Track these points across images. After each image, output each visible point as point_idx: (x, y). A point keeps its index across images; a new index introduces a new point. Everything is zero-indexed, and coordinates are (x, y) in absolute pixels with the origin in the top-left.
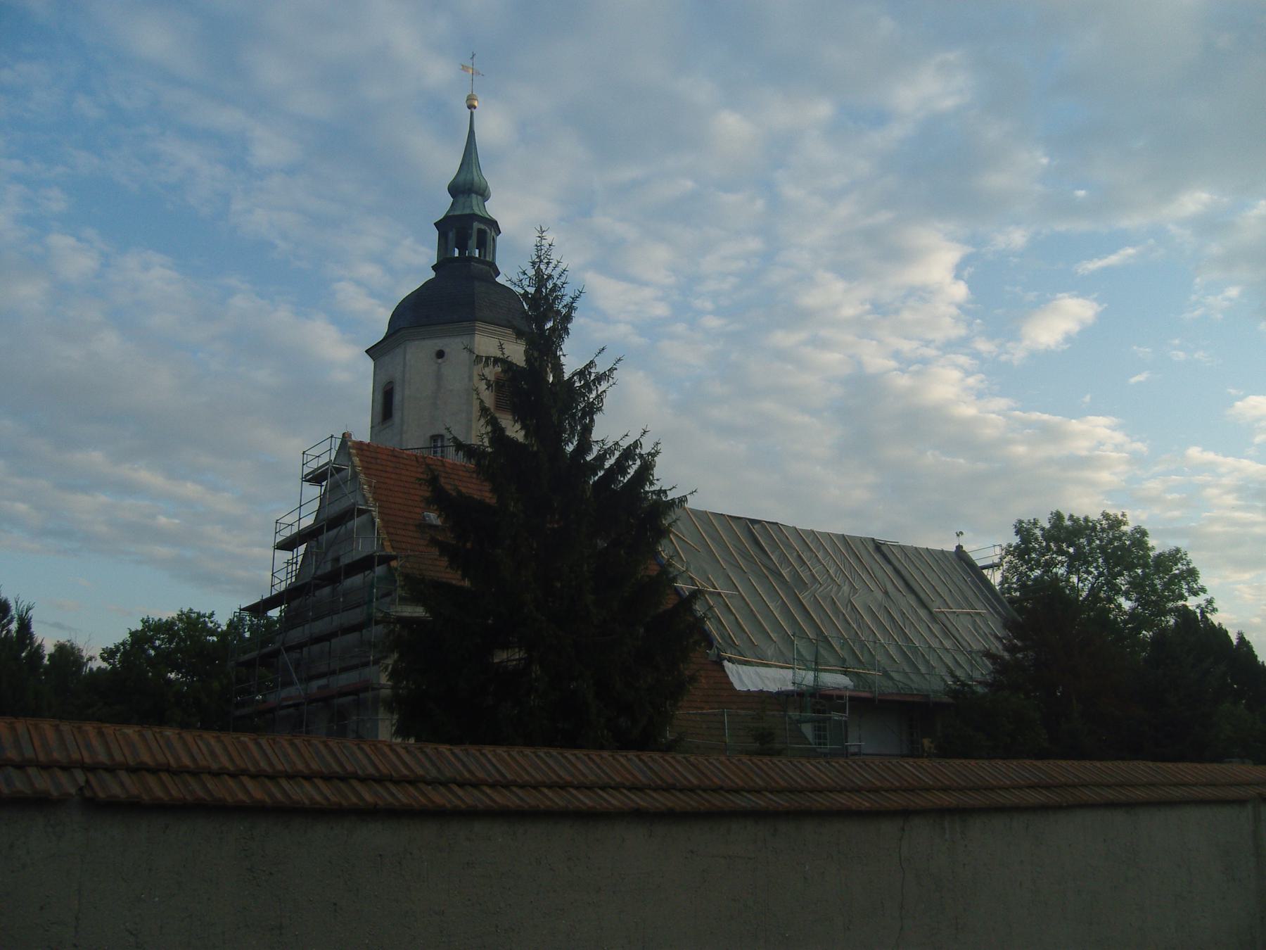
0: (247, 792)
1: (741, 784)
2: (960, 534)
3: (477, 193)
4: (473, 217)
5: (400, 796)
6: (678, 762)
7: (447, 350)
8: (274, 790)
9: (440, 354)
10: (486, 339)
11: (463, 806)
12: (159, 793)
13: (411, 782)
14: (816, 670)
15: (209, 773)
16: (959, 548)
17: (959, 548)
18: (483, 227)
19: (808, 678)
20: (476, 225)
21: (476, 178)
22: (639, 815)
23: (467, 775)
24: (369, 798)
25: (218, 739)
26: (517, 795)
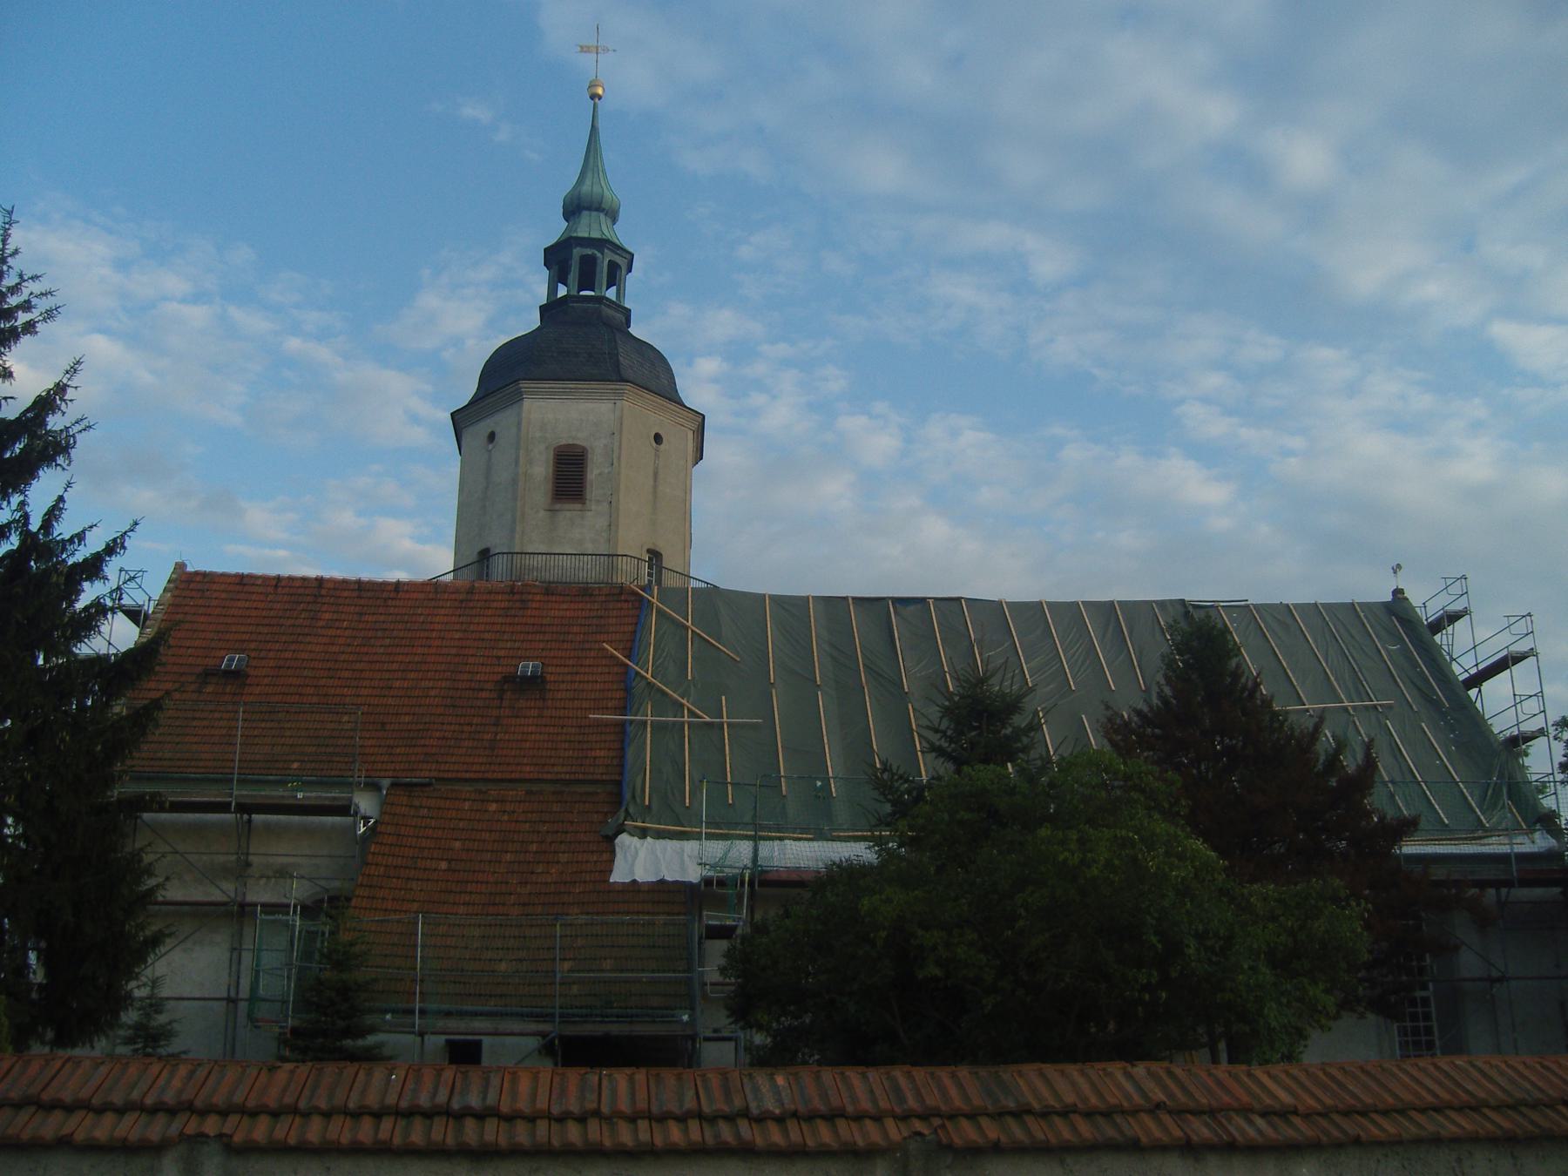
0: (1165, 1129)
1: (1446, 1096)
2: (1397, 568)
3: (589, 209)
4: (603, 243)
5: (1464, 1123)
6: (1423, 1070)
7: (497, 430)
8: (1519, 1119)
9: (492, 437)
10: (542, 403)
11: (1499, 1133)
12: (1157, 1133)
13: (1436, 1110)
14: (755, 839)
15: (988, 1115)
16: (1398, 592)
17: (1398, 592)
18: (589, 251)
19: (741, 851)
20: (577, 252)
21: (607, 193)
22: (1393, 1144)
23: (1390, 1100)
24: (1506, 1124)
25: (1083, 1073)
26: (1376, 1124)
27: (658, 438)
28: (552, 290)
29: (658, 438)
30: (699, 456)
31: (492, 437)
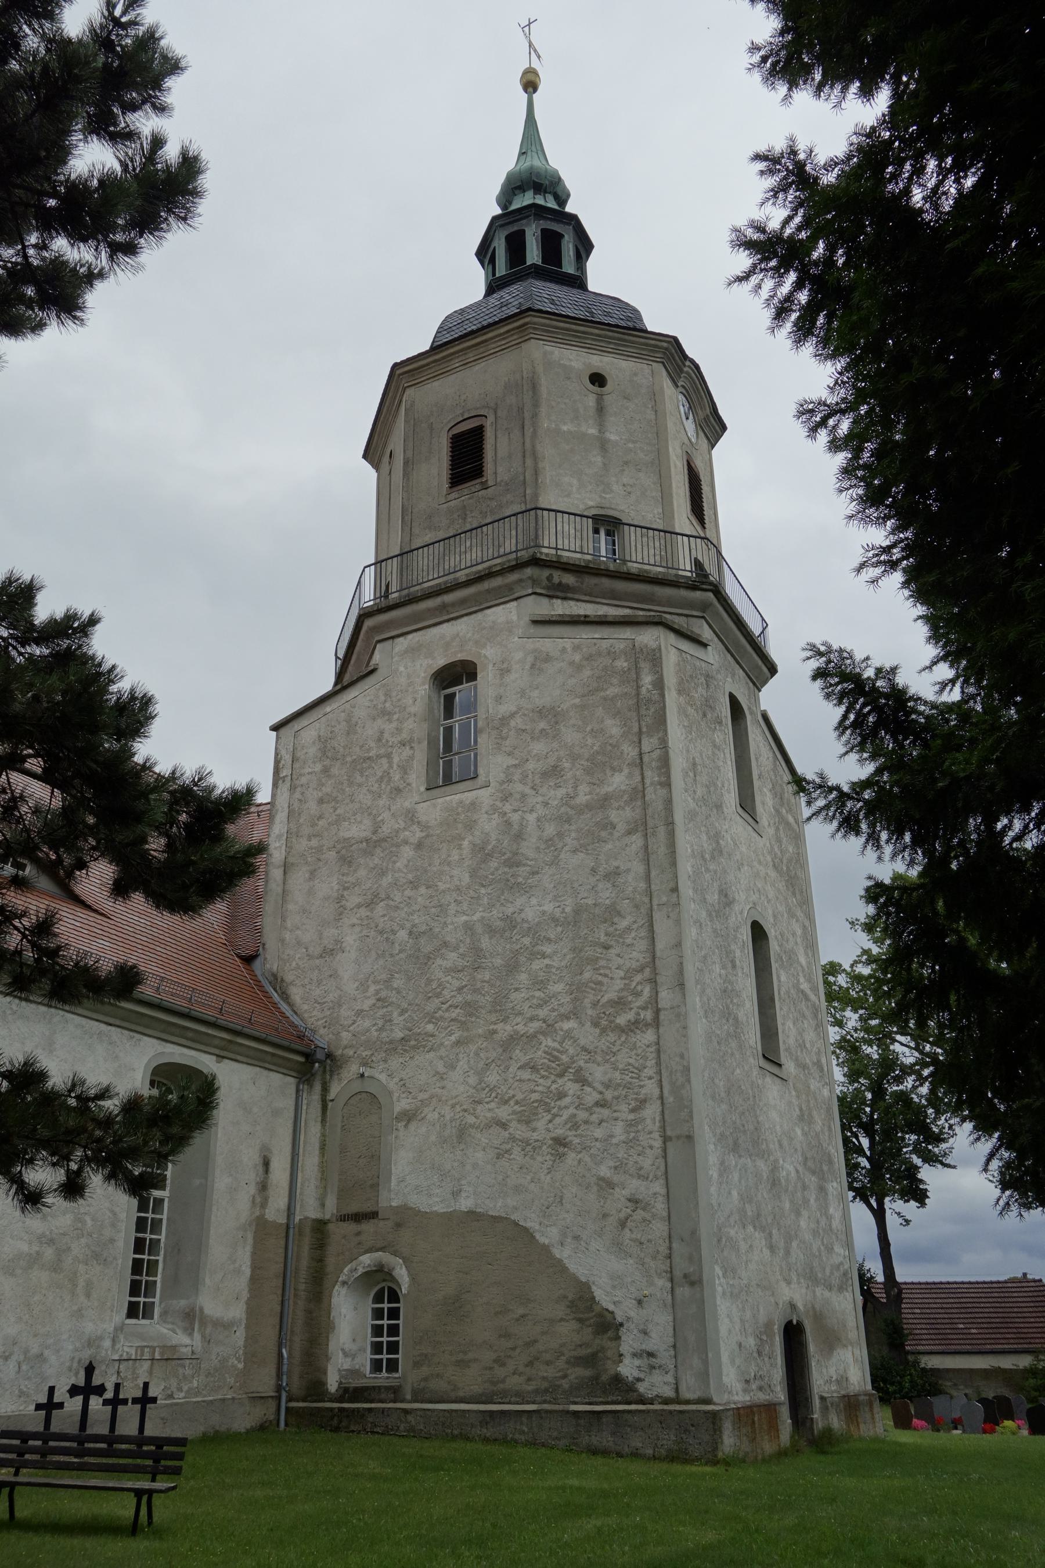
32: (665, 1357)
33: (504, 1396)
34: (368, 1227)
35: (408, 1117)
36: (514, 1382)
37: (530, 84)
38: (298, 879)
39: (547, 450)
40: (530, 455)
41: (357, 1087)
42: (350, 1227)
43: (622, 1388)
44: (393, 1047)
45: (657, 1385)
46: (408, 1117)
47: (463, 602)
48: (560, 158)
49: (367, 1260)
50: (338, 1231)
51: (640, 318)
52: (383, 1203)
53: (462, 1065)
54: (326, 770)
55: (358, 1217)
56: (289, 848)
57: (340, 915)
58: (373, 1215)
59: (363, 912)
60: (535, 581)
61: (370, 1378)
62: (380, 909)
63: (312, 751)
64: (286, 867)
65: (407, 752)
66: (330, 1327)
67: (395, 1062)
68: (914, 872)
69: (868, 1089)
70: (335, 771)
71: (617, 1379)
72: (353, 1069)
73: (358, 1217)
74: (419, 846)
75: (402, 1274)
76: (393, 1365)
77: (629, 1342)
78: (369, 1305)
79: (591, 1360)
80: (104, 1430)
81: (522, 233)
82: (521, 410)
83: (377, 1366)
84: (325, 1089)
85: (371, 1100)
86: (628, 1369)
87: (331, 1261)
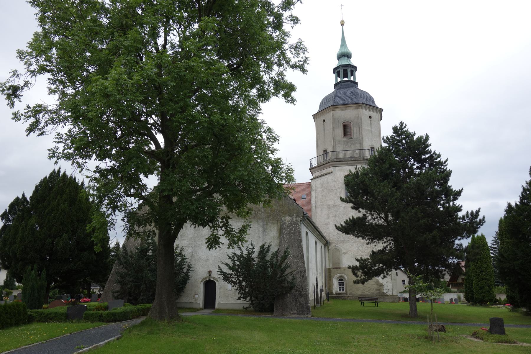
9: (324, 121)
27: (370, 117)
28: (336, 79)
29: (370, 117)
30: (381, 119)
31: (324, 121)
32: (391, 290)
33: (365, 295)
34: (339, 270)
35: (345, 253)
36: (366, 293)
37: (343, 25)
38: (319, 210)
39: (364, 133)
40: (360, 133)
41: (335, 247)
42: (336, 270)
43: (384, 293)
44: (341, 242)
45: (389, 293)
46: (345, 253)
47: (351, 163)
48: (351, 48)
49: (339, 275)
50: (333, 270)
51: (373, 101)
52: (341, 266)
53: (355, 246)
54: (323, 190)
55: (337, 268)
56: (316, 204)
57: (328, 218)
58: (340, 268)
59: (333, 218)
60: (366, 163)
61: (339, 292)
62: (337, 218)
63: (319, 186)
64: (316, 207)
65: (340, 190)
66: (333, 284)
67: (342, 244)
68: (457, 242)
69: (88, 129)
70: (325, 190)
71: (383, 293)
72: (333, 245)
73: (337, 268)
74: (344, 208)
75: (346, 277)
76: (343, 290)
77: (385, 288)
78: (338, 281)
79: (379, 290)
80: (408, 304)
81: (347, 70)
82: (359, 124)
83: (340, 290)
84: (328, 247)
85: (338, 250)
86: (385, 291)
87: (332, 275)
